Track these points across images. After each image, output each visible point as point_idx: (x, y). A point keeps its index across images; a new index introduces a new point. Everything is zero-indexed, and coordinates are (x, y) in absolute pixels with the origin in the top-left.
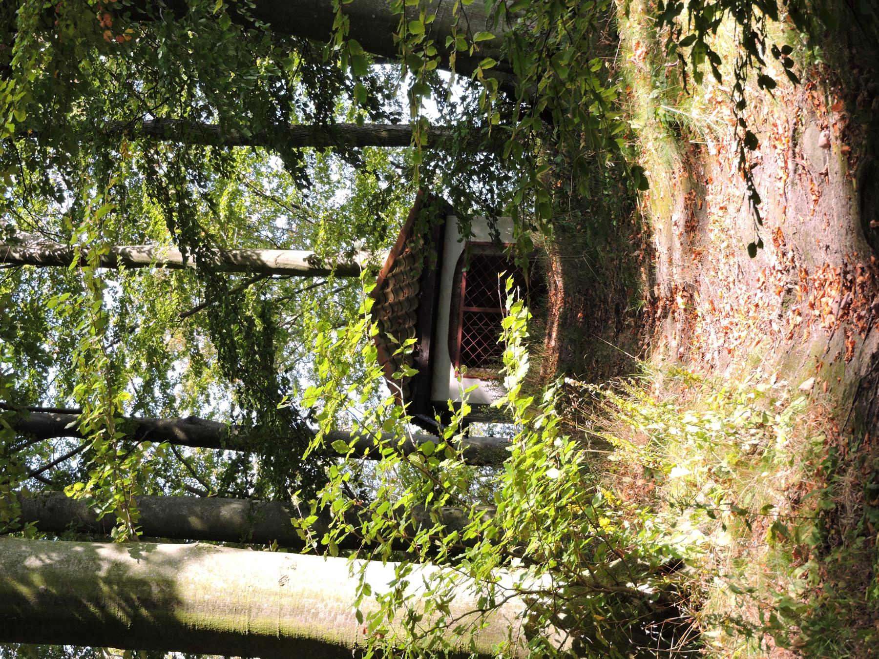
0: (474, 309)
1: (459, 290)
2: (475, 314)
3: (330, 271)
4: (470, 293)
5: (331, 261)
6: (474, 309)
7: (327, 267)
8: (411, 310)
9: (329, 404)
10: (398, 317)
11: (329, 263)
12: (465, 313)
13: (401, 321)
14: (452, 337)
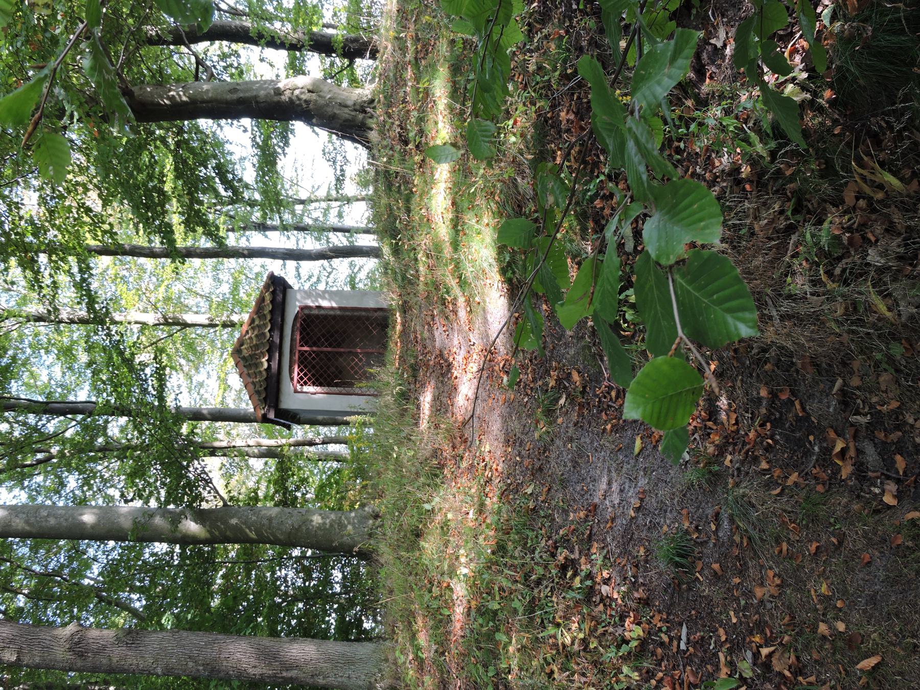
0: (306, 348)
2: (306, 351)
4: (302, 339)
6: (306, 348)
7: (218, 322)
10: (255, 354)
12: (300, 351)
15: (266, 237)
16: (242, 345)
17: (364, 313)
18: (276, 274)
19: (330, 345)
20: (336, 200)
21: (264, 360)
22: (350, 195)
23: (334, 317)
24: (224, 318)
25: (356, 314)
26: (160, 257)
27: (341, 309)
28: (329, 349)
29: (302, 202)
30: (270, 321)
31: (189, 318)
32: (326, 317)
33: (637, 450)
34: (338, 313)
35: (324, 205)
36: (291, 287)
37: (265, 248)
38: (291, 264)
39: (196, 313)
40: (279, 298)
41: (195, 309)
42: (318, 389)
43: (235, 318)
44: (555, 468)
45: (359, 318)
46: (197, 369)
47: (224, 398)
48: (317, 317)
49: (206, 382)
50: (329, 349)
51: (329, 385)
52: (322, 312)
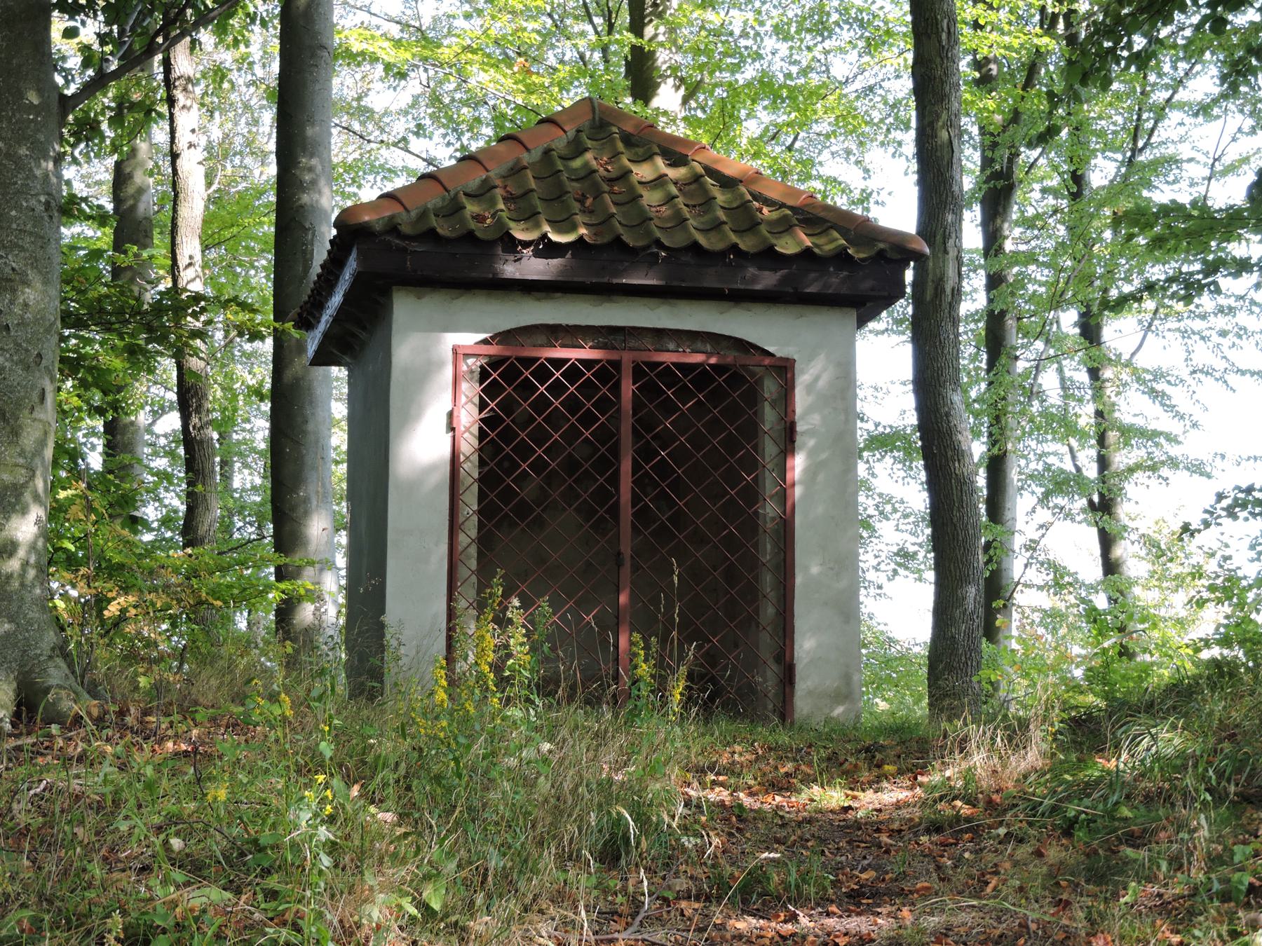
0: (628, 388)
1: (671, 346)
2: (616, 389)
3: (642, 37)
4: (667, 373)
5: (661, 38)
6: (628, 388)
7: (649, 31)
8: (621, 230)
9: (387, 44)
10: (598, 195)
11: (656, 35)
12: (616, 365)
13: (589, 202)
14: (556, 333)
16: (628, 140)
17: (769, 611)
20: (1103, 463)
21: (583, 231)
22: (1124, 510)
23: (752, 495)
24: (663, 58)
25: (768, 581)
27: (785, 529)
28: (626, 466)
29: (1090, 331)
30: (734, 248)
34: (770, 509)
35: (1085, 415)
36: (861, 323)
40: (835, 281)
42: (468, 445)
45: (752, 594)
48: (752, 430)
50: (626, 466)
52: (770, 449)
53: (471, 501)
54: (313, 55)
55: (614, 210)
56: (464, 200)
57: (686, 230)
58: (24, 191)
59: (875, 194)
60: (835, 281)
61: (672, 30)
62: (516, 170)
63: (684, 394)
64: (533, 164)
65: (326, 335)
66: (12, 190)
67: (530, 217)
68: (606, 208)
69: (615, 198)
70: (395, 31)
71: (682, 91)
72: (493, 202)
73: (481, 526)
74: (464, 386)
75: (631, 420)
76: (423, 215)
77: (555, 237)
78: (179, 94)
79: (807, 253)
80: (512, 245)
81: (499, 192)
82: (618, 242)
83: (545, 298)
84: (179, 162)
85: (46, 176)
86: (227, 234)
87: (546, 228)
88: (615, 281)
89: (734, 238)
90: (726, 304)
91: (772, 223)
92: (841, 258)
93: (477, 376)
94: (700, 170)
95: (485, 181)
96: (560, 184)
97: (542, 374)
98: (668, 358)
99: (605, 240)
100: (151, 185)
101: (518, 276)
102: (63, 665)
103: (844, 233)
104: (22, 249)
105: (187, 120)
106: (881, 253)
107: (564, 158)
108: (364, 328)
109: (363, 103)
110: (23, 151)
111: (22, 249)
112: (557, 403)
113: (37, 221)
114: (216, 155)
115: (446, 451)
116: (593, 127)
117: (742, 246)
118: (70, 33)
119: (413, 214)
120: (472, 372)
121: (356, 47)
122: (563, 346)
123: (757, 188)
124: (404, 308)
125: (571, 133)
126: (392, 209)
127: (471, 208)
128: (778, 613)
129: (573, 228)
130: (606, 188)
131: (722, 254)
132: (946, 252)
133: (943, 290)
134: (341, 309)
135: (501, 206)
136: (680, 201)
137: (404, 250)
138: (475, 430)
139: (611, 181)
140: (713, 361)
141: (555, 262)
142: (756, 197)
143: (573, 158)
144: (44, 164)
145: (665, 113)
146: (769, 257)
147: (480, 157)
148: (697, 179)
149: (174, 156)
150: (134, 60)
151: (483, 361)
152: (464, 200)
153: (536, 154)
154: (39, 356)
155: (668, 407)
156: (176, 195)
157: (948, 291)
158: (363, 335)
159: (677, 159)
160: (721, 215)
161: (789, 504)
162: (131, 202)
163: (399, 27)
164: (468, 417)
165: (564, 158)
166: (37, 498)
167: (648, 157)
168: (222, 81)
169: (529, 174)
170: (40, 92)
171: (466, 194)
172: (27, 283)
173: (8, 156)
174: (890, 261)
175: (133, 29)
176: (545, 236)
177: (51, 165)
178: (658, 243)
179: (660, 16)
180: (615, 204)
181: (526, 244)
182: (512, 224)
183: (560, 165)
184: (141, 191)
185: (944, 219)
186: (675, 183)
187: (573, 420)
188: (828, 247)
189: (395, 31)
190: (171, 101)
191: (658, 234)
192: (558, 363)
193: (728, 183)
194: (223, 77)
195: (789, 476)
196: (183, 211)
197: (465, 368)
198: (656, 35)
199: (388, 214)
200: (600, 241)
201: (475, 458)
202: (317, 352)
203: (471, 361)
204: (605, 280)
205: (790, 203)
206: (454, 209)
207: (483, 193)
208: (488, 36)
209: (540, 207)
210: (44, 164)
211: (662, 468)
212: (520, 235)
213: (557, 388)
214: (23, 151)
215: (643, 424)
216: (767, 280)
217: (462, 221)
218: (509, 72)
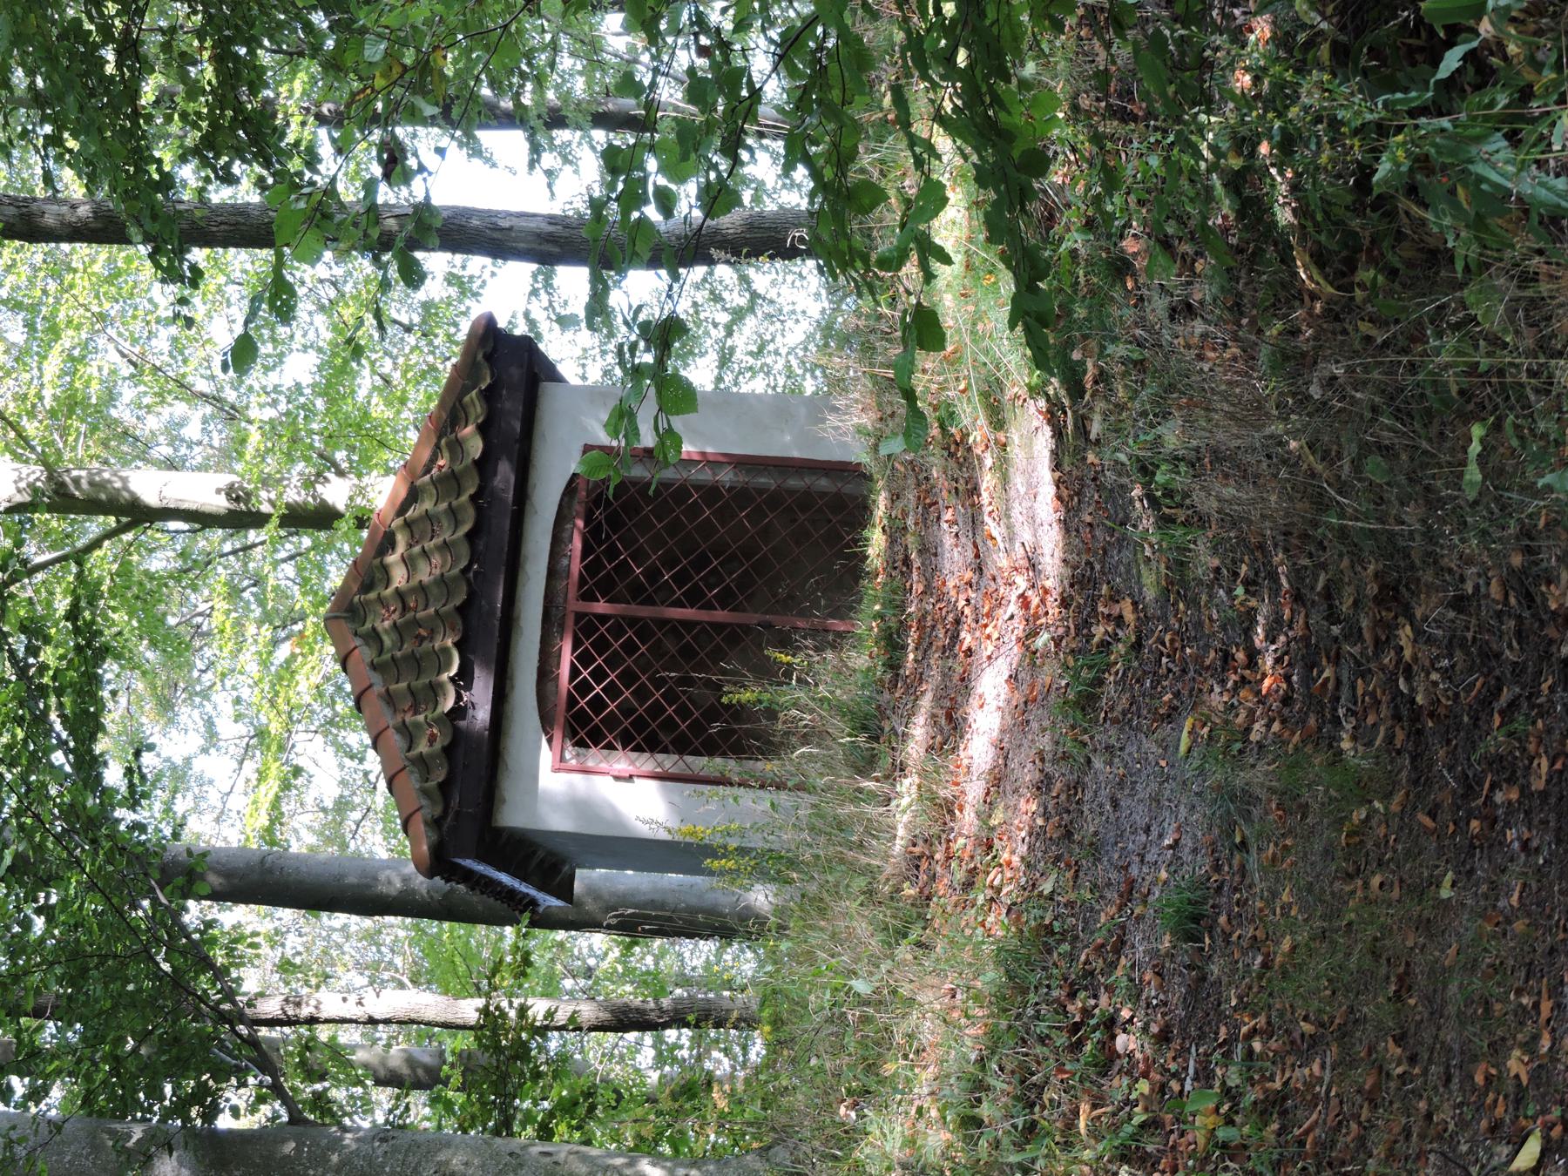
0: (601, 607)
1: (565, 562)
2: (603, 618)
4: (591, 569)
5: (273, 496)
6: (601, 607)
7: (265, 508)
8: (450, 606)
9: (263, 787)
10: (416, 623)
11: (270, 501)
12: (579, 616)
13: (423, 632)
14: (545, 673)
15: (476, 151)
16: (367, 587)
17: (823, 483)
18: (502, 324)
19: (725, 600)
23: (711, 492)
24: (294, 495)
25: (793, 483)
26: (58, 239)
28: (720, 615)
30: (473, 498)
31: (148, 486)
32: (680, 492)
33: (1183, 748)
34: (726, 476)
36: (553, 375)
37: (468, 213)
38: (573, 281)
39: (171, 465)
40: (511, 405)
41: (163, 450)
42: (646, 763)
43: (336, 492)
44: (1149, 858)
45: (806, 500)
46: (166, 706)
47: (276, 816)
49: (199, 764)
50: (720, 615)
51: (682, 747)
53: (700, 764)
54: (270, 871)
55: (432, 610)
56: (414, 753)
57: (454, 543)
58: (369, 1159)
59: (455, 271)
60: (511, 405)
61: (266, 482)
62: (389, 699)
63: (612, 553)
64: (385, 681)
65: (540, 889)
66: (367, 1169)
67: (435, 690)
68: (429, 616)
69: (421, 607)
70: (250, 767)
71: (331, 476)
72: (417, 725)
73: (724, 755)
74: (590, 764)
75: (633, 606)
76: (425, 793)
77: (454, 670)
78: (305, 1012)
79: (483, 429)
80: (459, 712)
81: (409, 718)
82: (462, 610)
83: (511, 679)
84: (377, 1016)
85: (358, 1140)
86: (462, 969)
87: (445, 677)
88: (499, 614)
89: (464, 498)
90: (528, 507)
91: (452, 459)
92: (489, 396)
93: (582, 750)
94: (400, 521)
95: (398, 730)
96: (405, 658)
97: (584, 688)
98: (576, 567)
99: (460, 622)
100: (398, 1050)
101: (488, 707)
102: (777, 1148)
103: (466, 390)
104: (419, 1164)
105: (330, 1003)
106: (488, 358)
107: (381, 652)
108: (534, 853)
109: (331, 806)
110: (335, 1158)
111: (419, 1164)
112: (612, 676)
113: (395, 1150)
114: (375, 974)
115: (653, 785)
116: (353, 620)
117: (472, 491)
118: (235, 1112)
119: (424, 802)
120: (578, 755)
121: (264, 821)
122: (558, 666)
123: (420, 469)
124: (513, 816)
125: (358, 642)
126: (419, 825)
127: (423, 747)
128: (826, 475)
129: (446, 651)
130: (409, 615)
131: (479, 511)
132: (511, 229)
133: (550, 234)
134: (514, 875)
135: (421, 718)
136: (429, 545)
137: (458, 814)
138: (635, 755)
139: (405, 608)
140: (580, 523)
141: (477, 672)
142: (428, 470)
143: (381, 642)
144: (347, 1142)
145: (351, 498)
146: (484, 465)
147: (375, 732)
148: (408, 525)
149: (372, 1021)
150: (264, 1059)
151: (568, 743)
152: (414, 753)
153: (376, 678)
154: (511, 1154)
155: (623, 568)
156: (413, 1022)
157: (551, 228)
158: (541, 854)
159: (388, 542)
160: (443, 506)
161: (721, 459)
162: (420, 1072)
163: (246, 763)
164: (622, 762)
165: (381, 652)
166: (632, 1164)
167: (386, 570)
168: (294, 965)
169: (393, 687)
170: (284, 1141)
171: (409, 750)
172: (447, 1163)
173: (338, 1171)
174: (495, 350)
175: (235, 1058)
176: (452, 679)
177: (349, 1135)
178: (465, 571)
179: (248, 494)
180: (426, 607)
181: (459, 697)
182: (439, 710)
183: (386, 656)
184: (411, 1061)
185: (476, 229)
186: (411, 546)
187: (598, 689)
188: (479, 410)
189: (250, 767)
190: (312, 1021)
191: (456, 571)
192: (575, 672)
193: (413, 495)
194: (289, 963)
195: (696, 458)
196: (430, 1015)
197: (574, 762)
198: (270, 501)
199: (422, 827)
200: (460, 626)
201: (660, 757)
202: (558, 897)
203: (568, 755)
204: (497, 623)
205: (434, 440)
206: (422, 763)
207: (409, 734)
208: (260, 680)
209: (424, 680)
210: (347, 1142)
211: (680, 579)
212: (449, 703)
213: (599, 675)
214: (335, 1158)
215: (637, 593)
216: (505, 474)
217: (432, 756)
218: (300, 659)
